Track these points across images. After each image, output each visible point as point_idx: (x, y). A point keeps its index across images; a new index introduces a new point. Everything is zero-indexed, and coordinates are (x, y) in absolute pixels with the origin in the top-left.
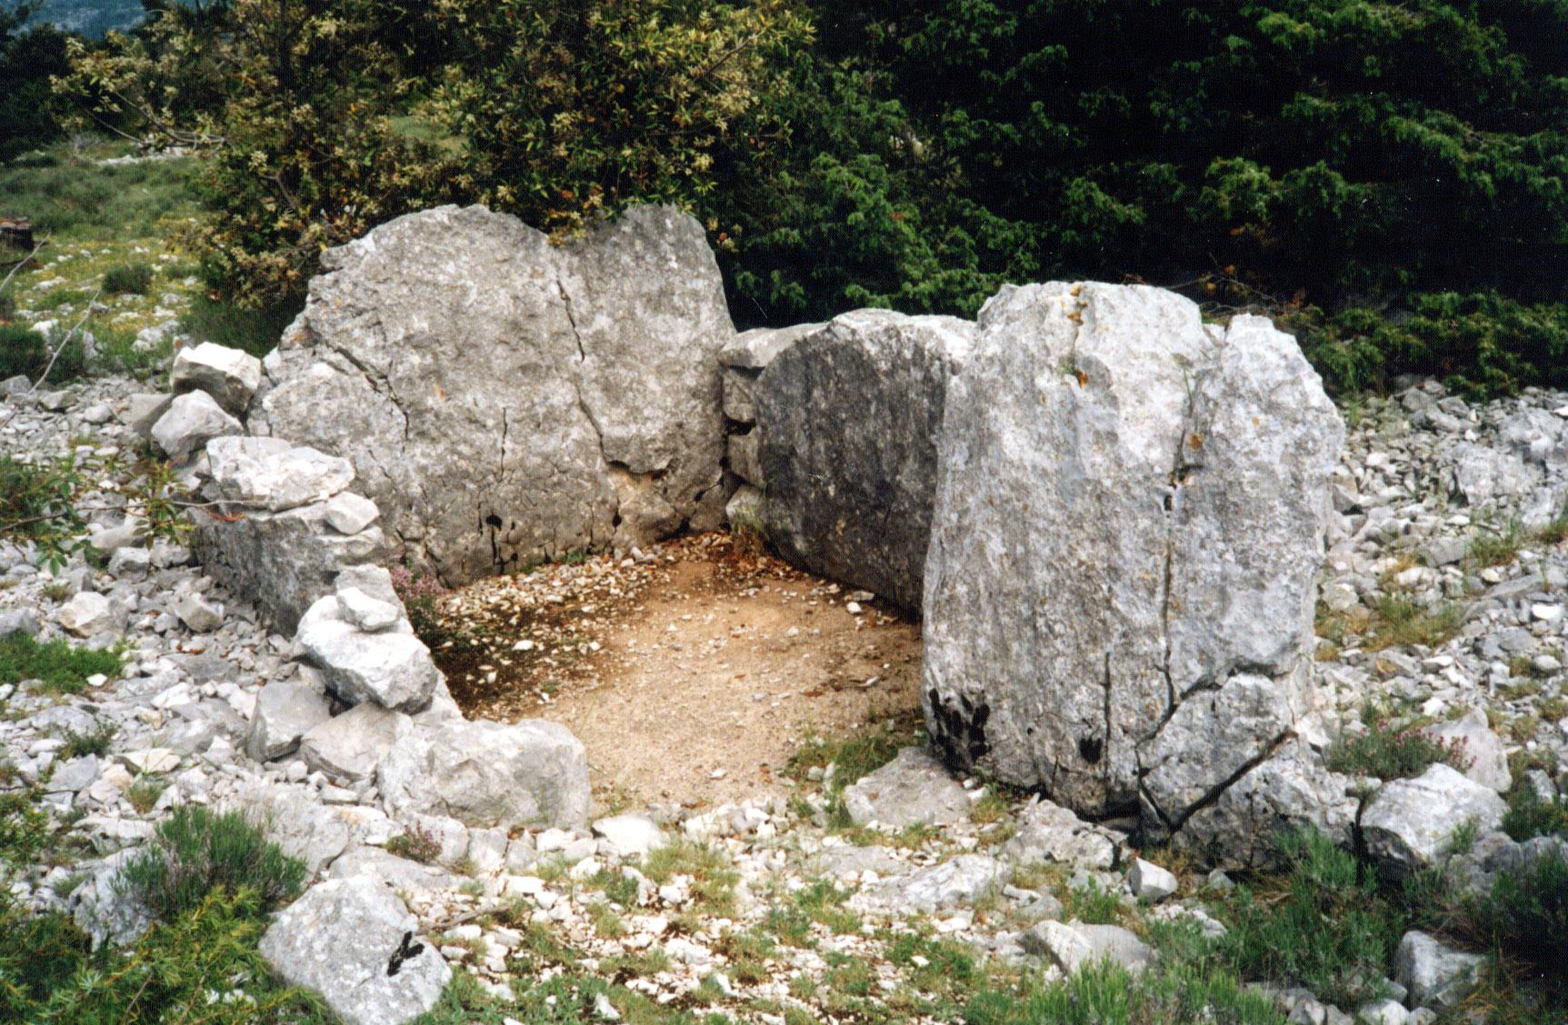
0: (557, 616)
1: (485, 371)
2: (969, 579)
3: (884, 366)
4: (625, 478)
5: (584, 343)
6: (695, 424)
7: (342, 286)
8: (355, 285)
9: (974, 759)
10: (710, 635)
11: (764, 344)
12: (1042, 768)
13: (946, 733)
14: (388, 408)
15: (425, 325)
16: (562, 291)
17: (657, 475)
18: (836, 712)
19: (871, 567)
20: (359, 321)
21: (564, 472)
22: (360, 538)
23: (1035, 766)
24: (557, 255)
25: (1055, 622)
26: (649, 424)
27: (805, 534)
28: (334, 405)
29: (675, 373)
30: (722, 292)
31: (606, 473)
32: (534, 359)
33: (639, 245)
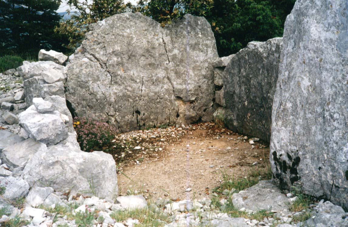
0: (151, 141)
1: (137, 65)
2: (293, 100)
3: (265, 55)
4: (181, 102)
5: (170, 58)
6: (204, 87)
7: (94, 34)
8: (98, 34)
9: (292, 183)
10: (200, 148)
11: (226, 60)
12: (325, 187)
13: (280, 172)
14: (106, 74)
15: (119, 48)
16: (163, 41)
17: (192, 102)
18: (239, 173)
19: (259, 129)
20: (99, 46)
21: (162, 99)
22: (53, 85)
23: (322, 186)
24: (163, 30)
25: (334, 113)
26: (189, 85)
27: (237, 120)
28: (88, 70)
29: (198, 70)
30: (215, 45)
31: (175, 100)
32: (153, 62)
33: (189, 28)
